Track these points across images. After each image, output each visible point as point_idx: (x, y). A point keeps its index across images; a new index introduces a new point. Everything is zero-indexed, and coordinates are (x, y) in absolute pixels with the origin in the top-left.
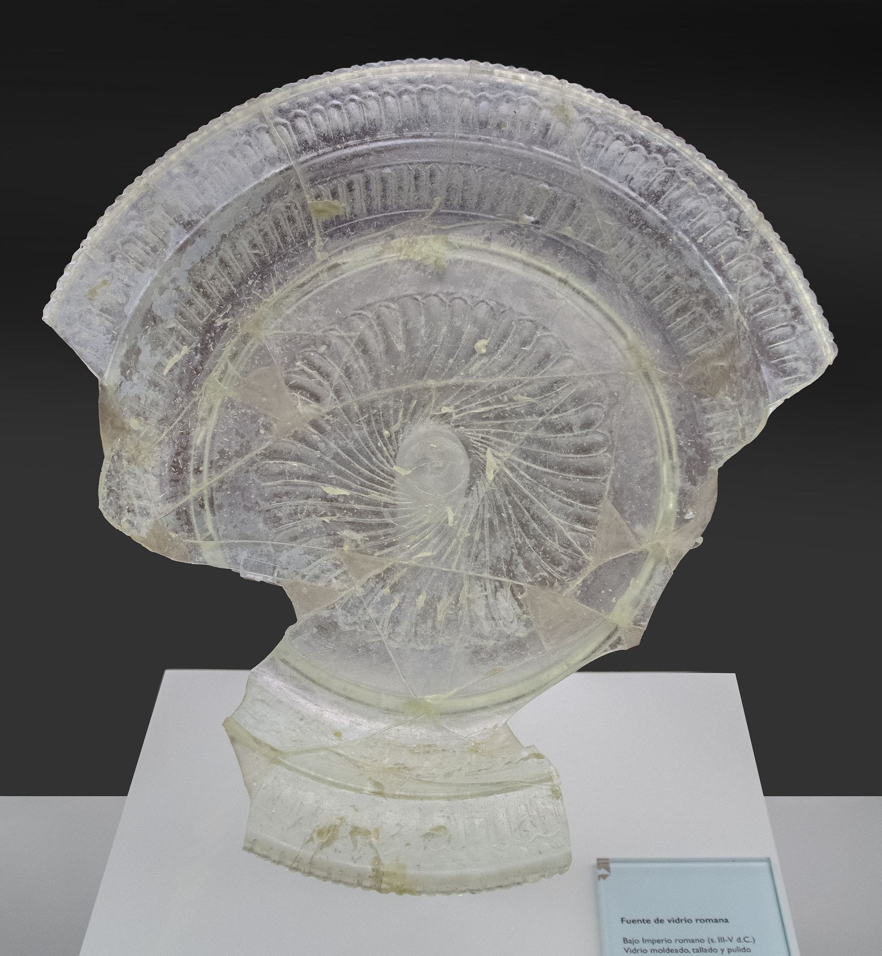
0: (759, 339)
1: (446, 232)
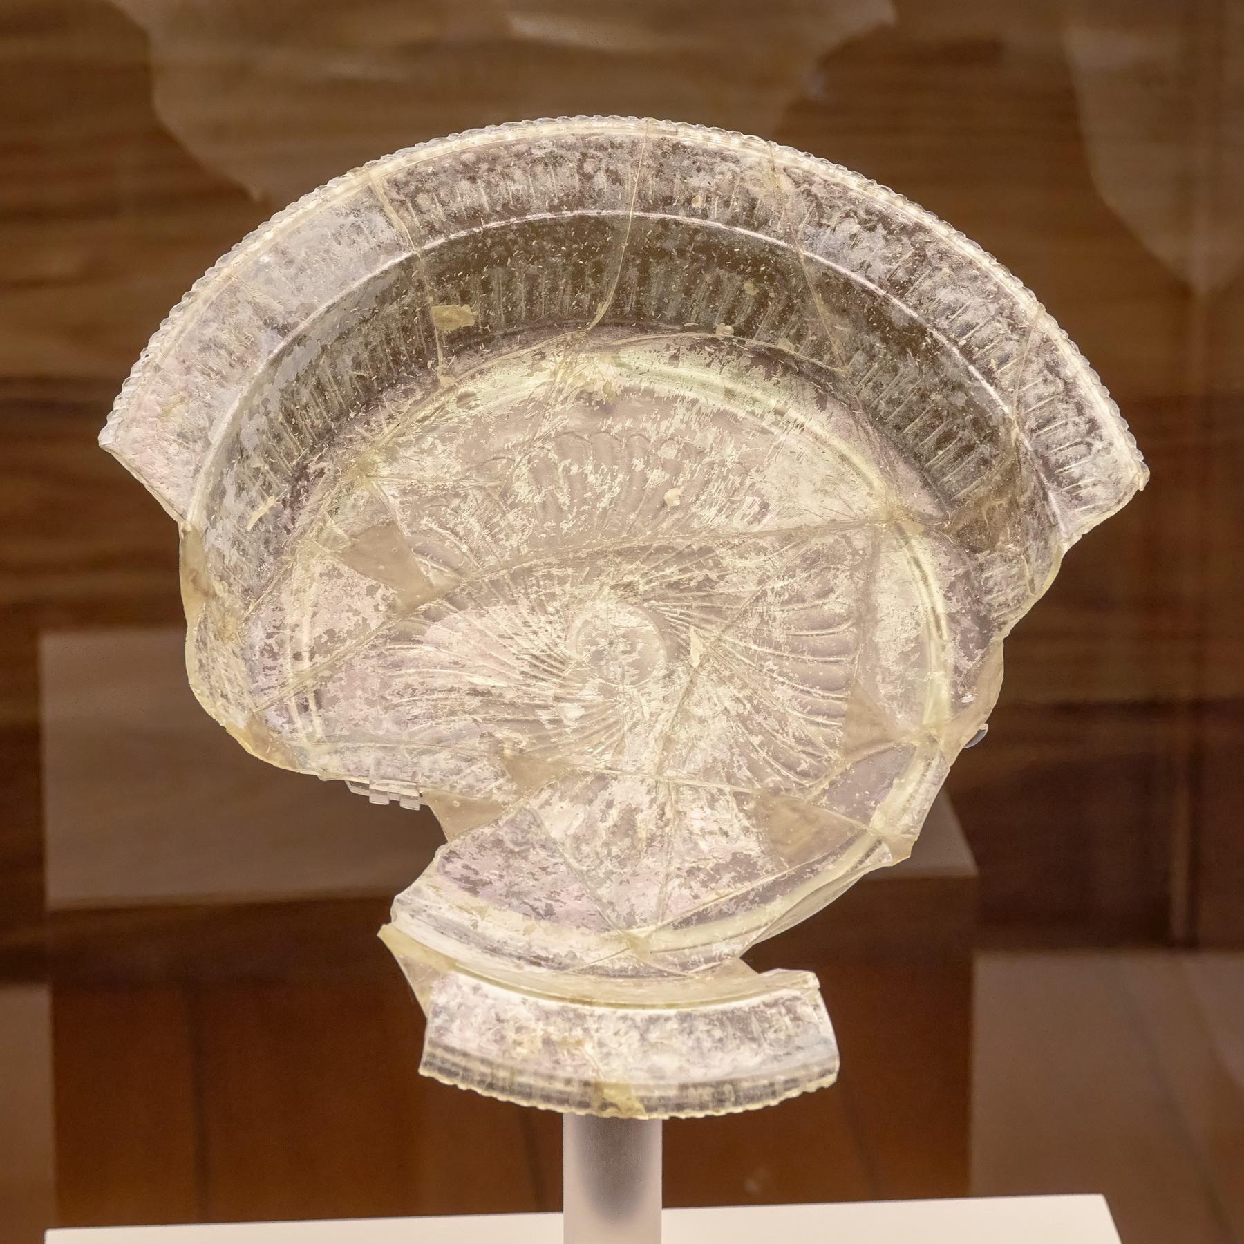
0: (1046, 462)
1: (616, 349)
